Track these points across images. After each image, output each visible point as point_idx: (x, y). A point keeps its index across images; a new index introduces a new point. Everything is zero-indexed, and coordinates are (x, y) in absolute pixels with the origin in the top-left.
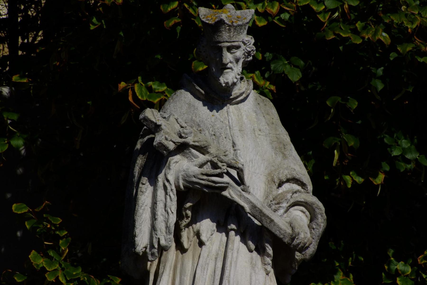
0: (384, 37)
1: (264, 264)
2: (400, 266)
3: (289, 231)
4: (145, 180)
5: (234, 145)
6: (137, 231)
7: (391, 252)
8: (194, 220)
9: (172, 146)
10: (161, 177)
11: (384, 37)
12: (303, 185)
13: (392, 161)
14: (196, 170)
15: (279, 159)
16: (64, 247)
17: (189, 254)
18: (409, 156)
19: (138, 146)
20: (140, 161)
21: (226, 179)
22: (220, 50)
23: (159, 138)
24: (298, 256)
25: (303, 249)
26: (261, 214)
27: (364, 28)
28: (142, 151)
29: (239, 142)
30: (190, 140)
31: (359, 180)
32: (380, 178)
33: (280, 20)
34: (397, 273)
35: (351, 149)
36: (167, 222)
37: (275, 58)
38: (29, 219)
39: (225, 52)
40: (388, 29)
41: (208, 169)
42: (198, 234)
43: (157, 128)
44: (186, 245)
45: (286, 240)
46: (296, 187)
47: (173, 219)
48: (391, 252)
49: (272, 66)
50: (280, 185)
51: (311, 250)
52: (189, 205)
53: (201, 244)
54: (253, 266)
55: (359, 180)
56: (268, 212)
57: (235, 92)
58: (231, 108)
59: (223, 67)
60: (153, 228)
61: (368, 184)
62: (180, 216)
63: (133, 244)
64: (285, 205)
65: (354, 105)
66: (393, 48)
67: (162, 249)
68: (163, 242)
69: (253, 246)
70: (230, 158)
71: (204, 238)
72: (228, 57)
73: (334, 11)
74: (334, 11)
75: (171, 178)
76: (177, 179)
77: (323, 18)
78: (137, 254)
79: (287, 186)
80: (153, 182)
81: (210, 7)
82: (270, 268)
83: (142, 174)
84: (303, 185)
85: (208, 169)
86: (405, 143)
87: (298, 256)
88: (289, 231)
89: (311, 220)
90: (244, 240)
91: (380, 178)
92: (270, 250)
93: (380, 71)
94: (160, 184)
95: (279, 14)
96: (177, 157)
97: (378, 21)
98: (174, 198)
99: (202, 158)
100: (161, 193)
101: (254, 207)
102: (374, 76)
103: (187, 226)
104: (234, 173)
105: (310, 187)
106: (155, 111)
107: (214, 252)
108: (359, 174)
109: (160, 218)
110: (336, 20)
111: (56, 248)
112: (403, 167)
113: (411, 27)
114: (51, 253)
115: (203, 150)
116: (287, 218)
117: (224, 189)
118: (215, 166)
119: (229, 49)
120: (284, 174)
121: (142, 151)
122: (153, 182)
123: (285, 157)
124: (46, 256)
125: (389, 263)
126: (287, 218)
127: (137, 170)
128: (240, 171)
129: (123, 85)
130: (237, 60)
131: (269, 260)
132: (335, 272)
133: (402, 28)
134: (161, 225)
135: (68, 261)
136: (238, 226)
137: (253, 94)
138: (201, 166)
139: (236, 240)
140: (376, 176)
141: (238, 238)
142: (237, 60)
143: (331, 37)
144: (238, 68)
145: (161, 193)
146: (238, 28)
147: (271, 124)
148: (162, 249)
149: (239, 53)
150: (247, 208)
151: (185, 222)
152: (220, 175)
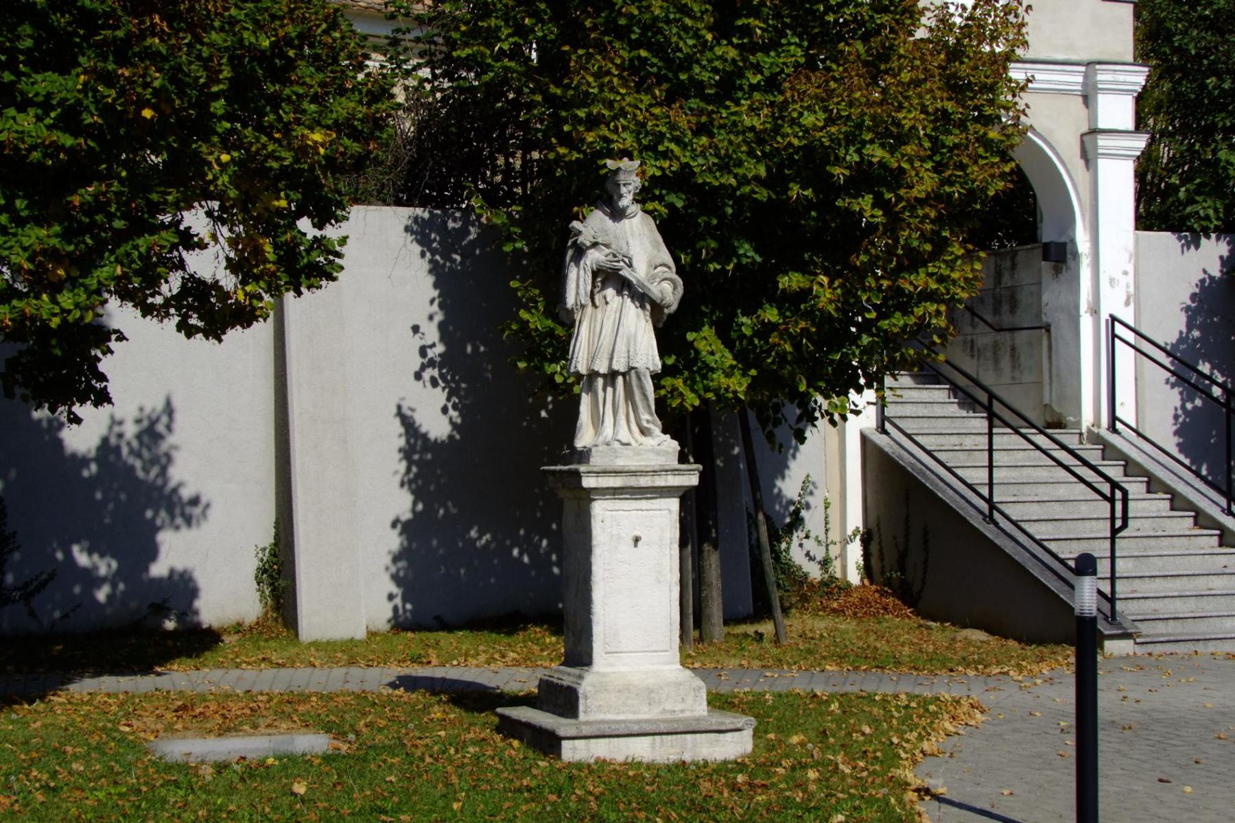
0: (733, 181)
1: (645, 315)
2: (745, 320)
3: (660, 295)
4: (572, 264)
5: (627, 243)
6: (567, 295)
7: (739, 311)
8: (603, 289)
9: (588, 244)
10: (582, 263)
11: (733, 181)
12: (669, 268)
13: (739, 257)
14: (603, 258)
15: (655, 252)
16: (541, 308)
17: (599, 310)
18: (748, 254)
19: (569, 244)
20: (570, 253)
21: (622, 264)
22: (619, 185)
23: (581, 239)
24: (666, 311)
25: (668, 307)
26: (643, 286)
27: (721, 176)
28: (571, 247)
29: (631, 241)
30: (600, 240)
31: (718, 267)
32: (730, 267)
33: (671, 171)
34: (743, 324)
35: (713, 249)
36: (585, 289)
37: (668, 194)
38: (520, 290)
39: (622, 187)
40: (736, 176)
41: (611, 257)
42: (605, 297)
43: (580, 232)
44: (597, 304)
45: (658, 301)
46: (665, 269)
47: (589, 288)
48: (739, 311)
49: (666, 198)
50: (656, 268)
51: (674, 307)
52: (599, 279)
53: (607, 303)
54: (638, 317)
55: (718, 267)
56: (647, 284)
57: (629, 211)
58: (626, 221)
59: (621, 196)
60: (577, 294)
61: (724, 271)
62: (594, 286)
63: (565, 303)
64: (658, 280)
65: (715, 222)
66: (738, 188)
67: (583, 306)
68: (583, 302)
69: (638, 305)
70: (624, 251)
71: (608, 299)
72: (624, 190)
73: (703, 166)
74: (703, 166)
75: (588, 263)
76: (592, 264)
77: (697, 170)
78: (567, 309)
79: (659, 269)
80: (578, 265)
81: (614, 159)
82: (649, 318)
83: (571, 261)
84: (669, 268)
85: (611, 257)
86: (747, 246)
87: (666, 311)
88: (660, 295)
89: (674, 289)
90: (633, 301)
91: (730, 267)
92: (648, 307)
93: (731, 203)
94: (582, 266)
95: (669, 168)
96: (592, 251)
97: (730, 172)
98: (590, 275)
99: (607, 251)
100: (582, 272)
101: (638, 281)
102: (727, 205)
103: (599, 292)
104: (627, 260)
105: (674, 269)
106: (579, 223)
107: (614, 310)
108: (719, 264)
109: (582, 287)
110: (704, 171)
111: (536, 308)
112: (745, 261)
113: (750, 176)
114: (533, 311)
115: (607, 246)
116: (659, 288)
117: (620, 270)
118: (615, 256)
119: (624, 185)
120: (659, 261)
121: (571, 247)
122: (578, 265)
123: (659, 251)
124: (530, 312)
125: (738, 317)
126: (659, 288)
127: (568, 258)
128: (630, 259)
129: (576, 209)
130: (630, 192)
131: (648, 313)
132: (703, 325)
133: (744, 176)
134: (582, 291)
135: (1189, 406)
136: (630, 291)
137: (640, 213)
138: (607, 256)
139: (628, 301)
140: (728, 265)
141: (629, 300)
142: (630, 192)
143: (700, 181)
144: (630, 197)
145: (582, 272)
146: (630, 172)
147: (651, 231)
148: (583, 306)
149: (630, 188)
150: (635, 282)
151: (597, 290)
152: (618, 262)
